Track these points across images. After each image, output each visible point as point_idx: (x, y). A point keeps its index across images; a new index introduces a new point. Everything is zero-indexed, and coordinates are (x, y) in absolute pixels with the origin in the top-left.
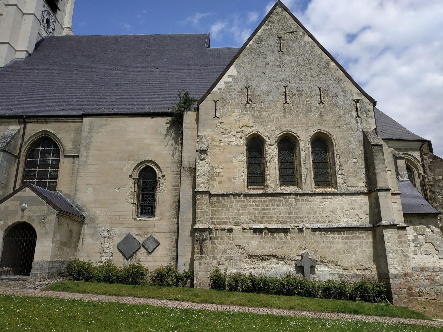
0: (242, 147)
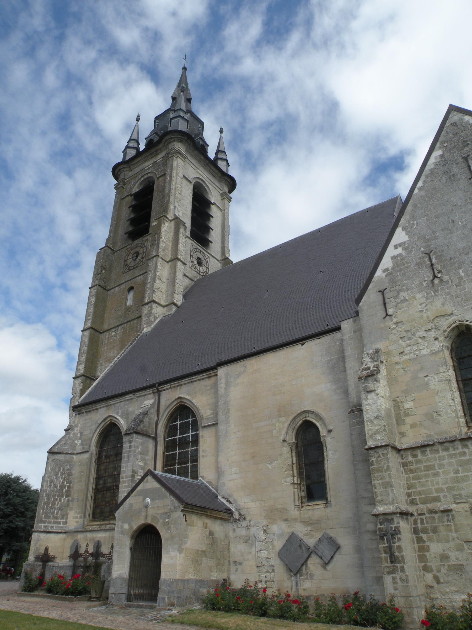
0: (441, 354)
